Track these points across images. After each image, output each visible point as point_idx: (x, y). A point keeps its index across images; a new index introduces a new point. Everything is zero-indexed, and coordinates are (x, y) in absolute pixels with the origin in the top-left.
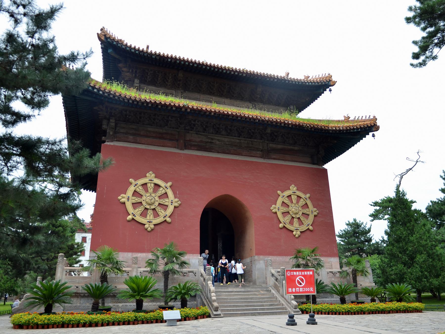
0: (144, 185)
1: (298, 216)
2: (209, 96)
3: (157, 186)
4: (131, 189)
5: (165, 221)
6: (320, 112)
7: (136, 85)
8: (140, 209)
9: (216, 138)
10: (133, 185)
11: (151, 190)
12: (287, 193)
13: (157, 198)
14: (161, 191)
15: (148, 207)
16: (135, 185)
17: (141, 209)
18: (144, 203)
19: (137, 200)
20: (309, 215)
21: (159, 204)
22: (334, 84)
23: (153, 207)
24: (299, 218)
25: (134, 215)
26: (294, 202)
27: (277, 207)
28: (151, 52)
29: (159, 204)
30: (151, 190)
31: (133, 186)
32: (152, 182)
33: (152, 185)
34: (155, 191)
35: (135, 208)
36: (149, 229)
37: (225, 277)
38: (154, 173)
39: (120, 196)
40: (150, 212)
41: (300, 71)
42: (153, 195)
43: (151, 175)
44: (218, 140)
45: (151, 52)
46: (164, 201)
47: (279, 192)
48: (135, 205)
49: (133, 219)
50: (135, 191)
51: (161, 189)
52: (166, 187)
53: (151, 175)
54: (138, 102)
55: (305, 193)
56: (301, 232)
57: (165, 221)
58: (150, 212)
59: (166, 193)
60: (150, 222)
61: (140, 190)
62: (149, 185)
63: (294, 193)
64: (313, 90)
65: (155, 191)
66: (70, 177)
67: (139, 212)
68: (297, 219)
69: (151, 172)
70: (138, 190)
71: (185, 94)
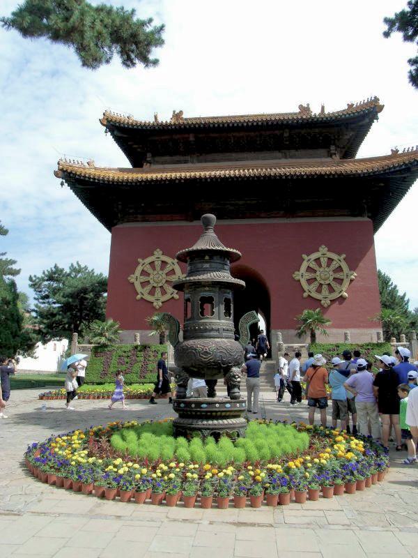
0: (152, 264)
1: (327, 282)
2: (228, 154)
3: (330, 260)
4: (139, 269)
5: (173, 297)
6: (375, 146)
7: (148, 159)
9: (228, 202)
11: (158, 268)
12: (314, 256)
15: (155, 285)
16: (308, 260)
20: (343, 280)
21: (167, 281)
22: (381, 108)
23: (160, 285)
24: (329, 285)
25: (142, 294)
26: (323, 265)
27: (302, 275)
28: (315, 115)
29: (167, 281)
30: (158, 268)
34: (162, 269)
35: (141, 274)
36: (157, 307)
38: (161, 250)
41: (330, 100)
42: (160, 272)
43: (323, 249)
44: (232, 205)
45: (315, 115)
47: (344, 256)
48: (143, 284)
49: (142, 298)
53: (323, 249)
54: (334, 175)
55: (339, 254)
56: (162, 303)
57: (173, 297)
60: (326, 298)
61: (313, 265)
63: (324, 254)
64: (357, 122)
65: (162, 269)
68: (326, 286)
69: (158, 250)
70: (145, 269)
71: (201, 158)
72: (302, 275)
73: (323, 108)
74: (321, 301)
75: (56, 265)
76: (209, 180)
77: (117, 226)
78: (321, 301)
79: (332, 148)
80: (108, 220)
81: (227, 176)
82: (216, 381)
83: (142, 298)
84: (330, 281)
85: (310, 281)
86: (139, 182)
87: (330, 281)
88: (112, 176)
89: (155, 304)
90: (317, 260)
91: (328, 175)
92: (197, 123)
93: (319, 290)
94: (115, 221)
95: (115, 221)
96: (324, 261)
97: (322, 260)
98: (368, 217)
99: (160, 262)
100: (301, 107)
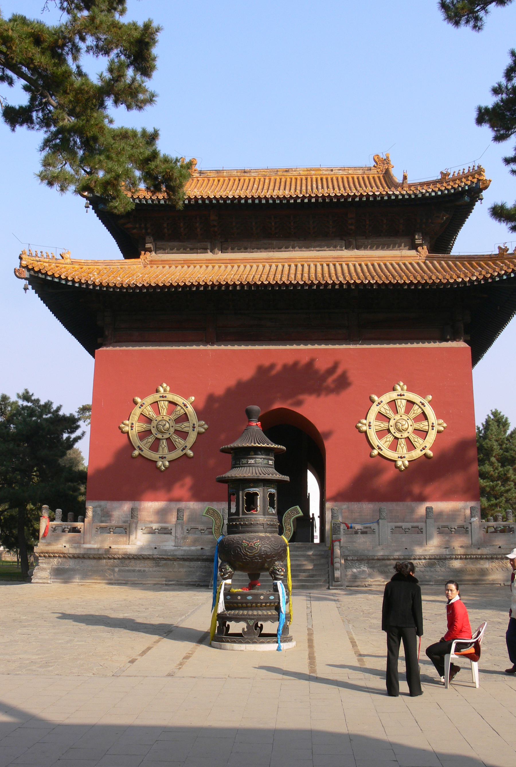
8: (382, 425)
10: (139, 405)
11: (412, 415)
13: (411, 429)
14: (423, 425)
15: (392, 430)
16: (381, 403)
17: (384, 425)
18: (392, 422)
19: (390, 413)
23: (398, 435)
30: (412, 415)
31: (182, 401)
32: (422, 406)
33: (420, 411)
34: (417, 419)
35: (377, 419)
37: (402, 640)
39: (167, 385)
40: (389, 438)
43: (401, 387)
46: (416, 440)
47: (430, 397)
50: (394, 400)
51: (426, 423)
52: (433, 426)
53: (401, 387)
57: (185, 454)
58: (389, 438)
59: (427, 432)
62: (416, 407)
65: (417, 419)
66: (442, 421)
67: (377, 428)
72: (371, 424)
73: (405, 178)
74: (156, 462)
75: (61, 406)
76: (238, 288)
77: (101, 349)
78: (156, 462)
79: (417, 237)
80: (91, 339)
81: (153, 285)
82: (259, 575)
83: (140, 454)
84: (409, 433)
85: (381, 434)
86: (132, 288)
87: (409, 433)
88: (96, 278)
89: (160, 463)
90: (393, 404)
91: (141, 288)
92: (278, 197)
93: (394, 447)
94: (99, 340)
95: (99, 340)
96: (402, 404)
97: (398, 402)
98: (465, 341)
99: (404, 402)
100: (442, 173)
